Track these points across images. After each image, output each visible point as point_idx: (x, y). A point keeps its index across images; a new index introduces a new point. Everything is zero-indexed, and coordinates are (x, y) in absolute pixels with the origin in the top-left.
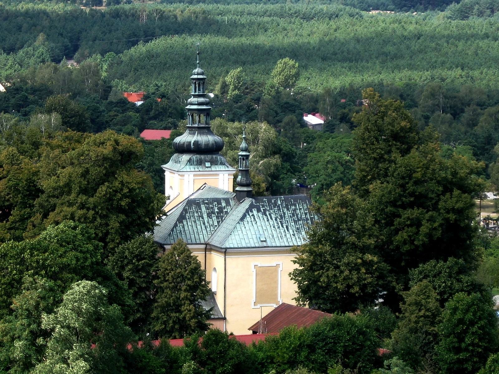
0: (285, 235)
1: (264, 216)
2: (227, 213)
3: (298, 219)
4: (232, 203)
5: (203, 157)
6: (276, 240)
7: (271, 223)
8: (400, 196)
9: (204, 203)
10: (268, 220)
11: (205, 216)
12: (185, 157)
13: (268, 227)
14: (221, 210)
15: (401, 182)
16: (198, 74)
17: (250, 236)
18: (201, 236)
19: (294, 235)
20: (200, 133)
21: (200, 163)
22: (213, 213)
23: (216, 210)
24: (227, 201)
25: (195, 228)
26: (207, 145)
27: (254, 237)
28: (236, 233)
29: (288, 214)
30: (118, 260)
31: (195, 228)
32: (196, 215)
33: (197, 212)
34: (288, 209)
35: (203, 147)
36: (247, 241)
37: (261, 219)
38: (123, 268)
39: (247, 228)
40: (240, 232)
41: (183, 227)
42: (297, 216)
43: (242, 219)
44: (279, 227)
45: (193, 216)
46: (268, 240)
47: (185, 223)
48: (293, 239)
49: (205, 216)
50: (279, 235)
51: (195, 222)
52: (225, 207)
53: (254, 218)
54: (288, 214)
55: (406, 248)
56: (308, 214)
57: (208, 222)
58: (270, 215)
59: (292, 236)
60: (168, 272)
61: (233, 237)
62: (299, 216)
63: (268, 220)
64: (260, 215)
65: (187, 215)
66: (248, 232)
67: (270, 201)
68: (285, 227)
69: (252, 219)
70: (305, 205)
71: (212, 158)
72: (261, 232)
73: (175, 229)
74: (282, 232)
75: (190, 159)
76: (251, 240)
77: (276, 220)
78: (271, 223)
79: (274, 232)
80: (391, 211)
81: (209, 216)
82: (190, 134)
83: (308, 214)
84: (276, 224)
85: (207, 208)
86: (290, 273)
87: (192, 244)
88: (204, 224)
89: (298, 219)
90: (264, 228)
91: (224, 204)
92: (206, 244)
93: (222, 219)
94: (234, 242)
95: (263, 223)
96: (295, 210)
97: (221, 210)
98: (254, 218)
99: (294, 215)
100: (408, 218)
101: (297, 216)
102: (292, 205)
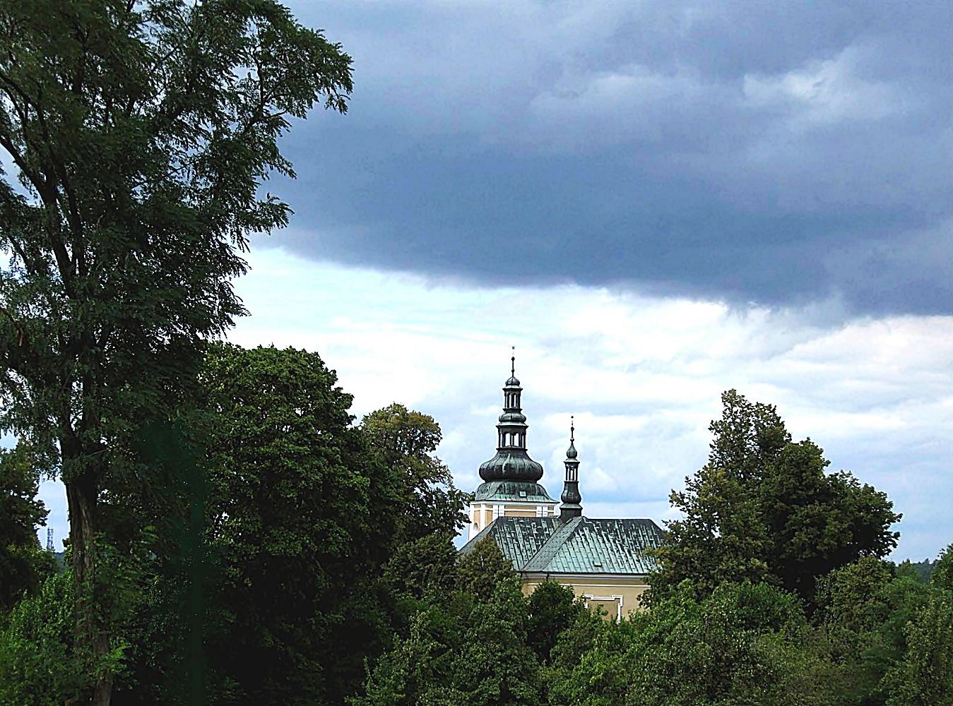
0: (627, 561)
1: (599, 537)
3: (641, 547)
4: (555, 524)
8: (795, 488)
11: (520, 537)
13: (605, 550)
14: (541, 532)
15: (795, 470)
17: (580, 560)
19: (639, 561)
21: (513, 491)
27: (586, 560)
29: (628, 541)
30: (400, 564)
32: (508, 536)
33: (510, 533)
34: (628, 536)
37: (595, 540)
38: (405, 575)
39: (577, 550)
42: (640, 545)
43: (570, 539)
45: (505, 538)
46: (604, 565)
48: (638, 565)
49: (520, 537)
50: (619, 560)
52: (546, 528)
53: (586, 539)
54: (628, 541)
55: (807, 554)
56: (654, 542)
57: (524, 546)
58: (606, 536)
59: (636, 562)
62: (643, 544)
65: (496, 535)
66: (579, 556)
68: (626, 551)
69: (583, 540)
70: (650, 532)
74: (623, 557)
75: (501, 486)
76: (571, 565)
80: (781, 507)
83: (654, 542)
84: (614, 547)
86: (640, 596)
88: (519, 547)
89: (641, 547)
90: (599, 551)
91: (544, 526)
93: (542, 543)
94: (560, 565)
95: (597, 545)
96: (637, 537)
97: (541, 532)
98: (586, 539)
99: (635, 542)
100: (808, 516)
101: (640, 545)
102: (632, 530)
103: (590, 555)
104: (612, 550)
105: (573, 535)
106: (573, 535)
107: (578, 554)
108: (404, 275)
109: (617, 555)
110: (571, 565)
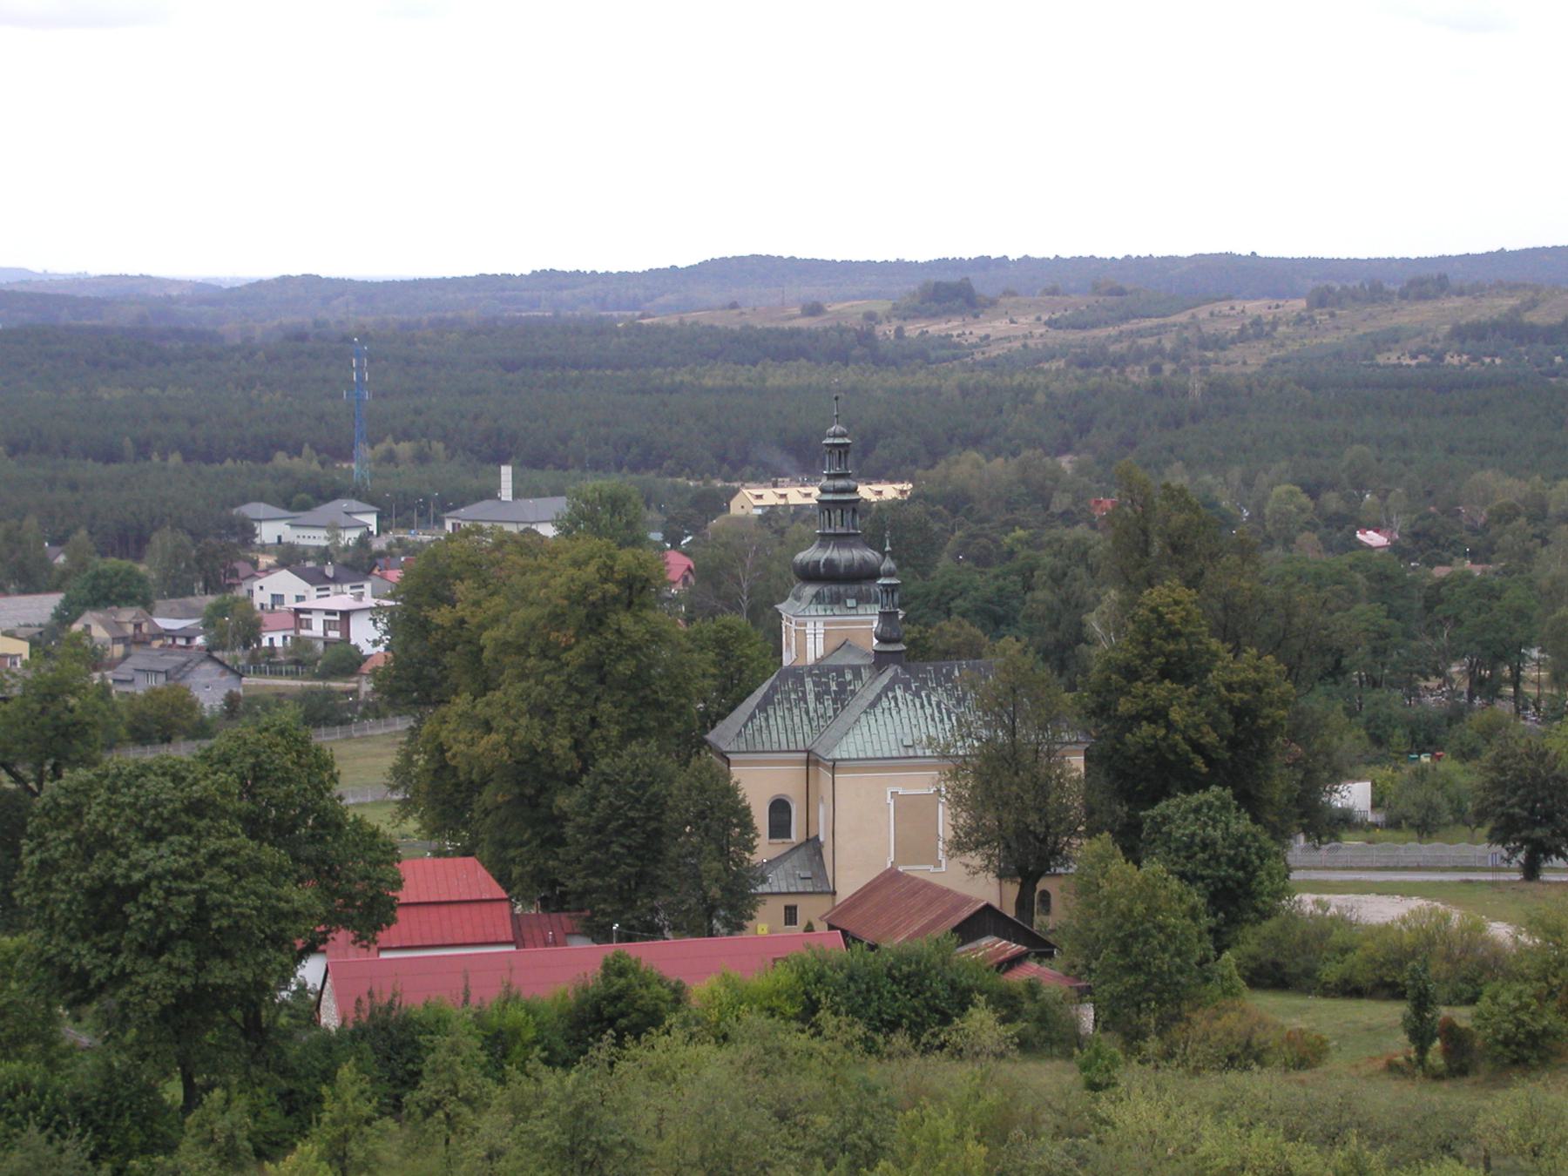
2: (853, 693)
4: (865, 674)
5: (842, 589)
7: (928, 711)
9: (810, 674)
10: (922, 707)
11: (811, 698)
12: (810, 590)
13: (922, 721)
14: (842, 686)
16: (835, 436)
17: (883, 737)
18: (800, 737)
20: (839, 546)
21: (837, 600)
22: (828, 692)
23: (834, 688)
24: (856, 671)
25: (788, 722)
26: (849, 567)
27: (892, 737)
28: (857, 731)
31: (788, 722)
32: (793, 696)
35: (842, 570)
36: (877, 747)
39: (881, 722)
41: (767, 719)
43: (873, 705)
44: (942, 721)
47: (771, 712)
49: (811, 698)
51: (790, 709)
60: (995, 784)
61: (850, 738)
63: (922, 707)
64: (909, 697)
67: (937, 671)
72: (907, 730)
76: (868, 746)
77: (938, 706)
78: (928, 711)
81: (819, 698)
82: (820, 546)
85: (816, 684)
87: (780, 752)
88: (807, 713)
90: (914, 722)
91: (849, 677)
92: (808, 752)
97: (842, 686)
103: (899, 730)
105: (879, 698)
106: (879, 698)
107: (882, 729)
108: (81, 281)
109: (939, 726)
110: (868, 746)
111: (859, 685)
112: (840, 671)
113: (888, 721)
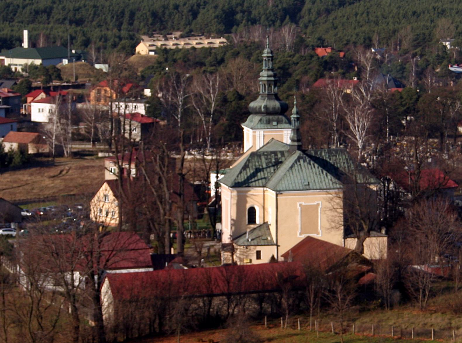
0: (325, 180)
4: (286, 154)
6: (317, 184)
7: (314, 170)
10: (312, 168)
17: (296, 181)
21: (269, 122)
24: (282, 153)
27: (300, 181)
35: (271, 109)
36: (294, 185)
39: (295, 175)
40: (289, 178)
46: (311, 184)
63: (312, 168)
71: (278, 118)
73: (239, 176)
78: (314, 170)
79: (316, 178)
85: (266, 159)
90: (308, 175)
91: (279, 156)
104: (316, 174)
109: (319, 176)
111: (283, 159)
112: (275, 153)
113: (298, 174)
